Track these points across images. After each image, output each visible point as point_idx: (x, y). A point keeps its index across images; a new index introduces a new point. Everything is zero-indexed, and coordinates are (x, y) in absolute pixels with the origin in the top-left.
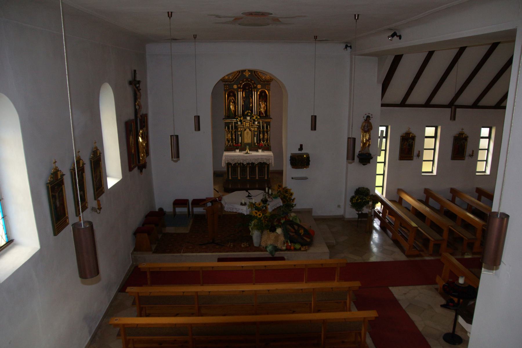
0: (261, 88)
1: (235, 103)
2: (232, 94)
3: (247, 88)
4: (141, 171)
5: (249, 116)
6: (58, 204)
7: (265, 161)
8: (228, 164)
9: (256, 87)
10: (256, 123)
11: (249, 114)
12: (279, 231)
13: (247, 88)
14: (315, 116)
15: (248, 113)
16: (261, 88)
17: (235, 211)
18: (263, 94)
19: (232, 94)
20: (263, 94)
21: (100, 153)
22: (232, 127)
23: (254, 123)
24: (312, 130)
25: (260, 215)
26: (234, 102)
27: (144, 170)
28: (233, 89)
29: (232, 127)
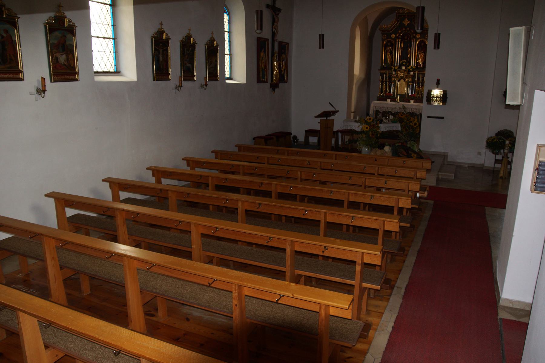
0: (420, 38)
1: (393, 54)
2: (389, 44)
3: (406, 37)
4: (274, 90)
5: (404, 65)
6: (161, 58)
7: (415, 111)
8: (377, 112)
9: (415, 37)
10: (412, 73)
11: (404, 63)
12: (387, 149)
13: (406, 37)
14: (439, 34)
15: (403, 62)
16: (420, 38)
17: (349, 128)
18: (422, 44)
19: (389, 44)
20: (422, 44)
21: (217, 46)
22: (386, 77)
23: (409, 74)
24: (435, 48)
25: (367, 128)
26: (391, 53)
27: (276, 90)
28: (391, 38)
29: (386, 77)
